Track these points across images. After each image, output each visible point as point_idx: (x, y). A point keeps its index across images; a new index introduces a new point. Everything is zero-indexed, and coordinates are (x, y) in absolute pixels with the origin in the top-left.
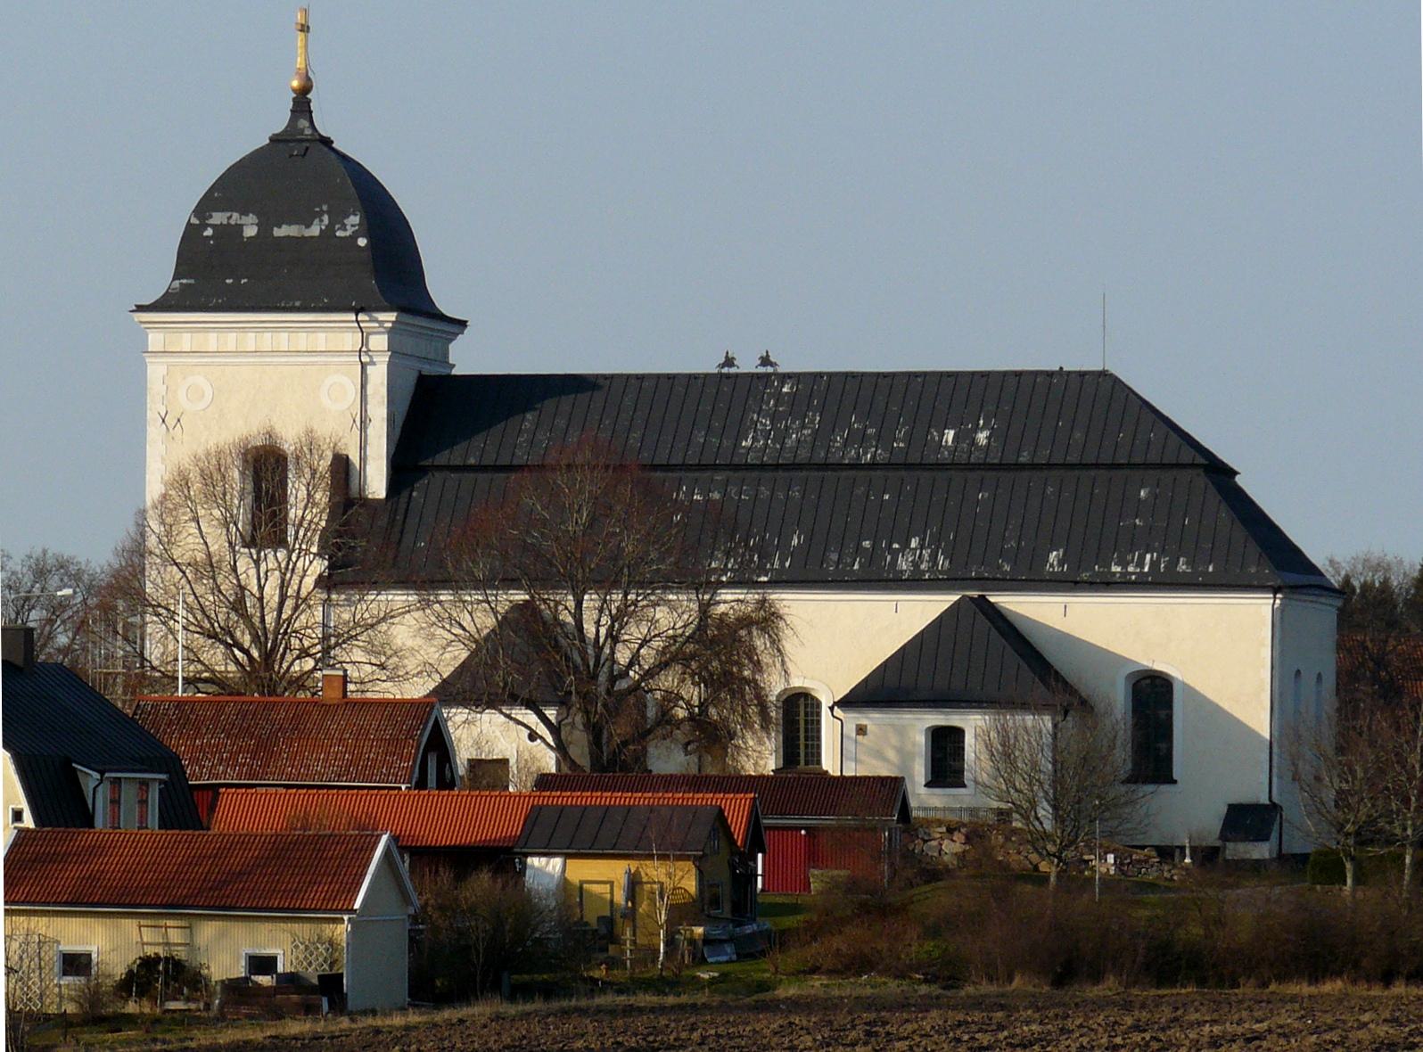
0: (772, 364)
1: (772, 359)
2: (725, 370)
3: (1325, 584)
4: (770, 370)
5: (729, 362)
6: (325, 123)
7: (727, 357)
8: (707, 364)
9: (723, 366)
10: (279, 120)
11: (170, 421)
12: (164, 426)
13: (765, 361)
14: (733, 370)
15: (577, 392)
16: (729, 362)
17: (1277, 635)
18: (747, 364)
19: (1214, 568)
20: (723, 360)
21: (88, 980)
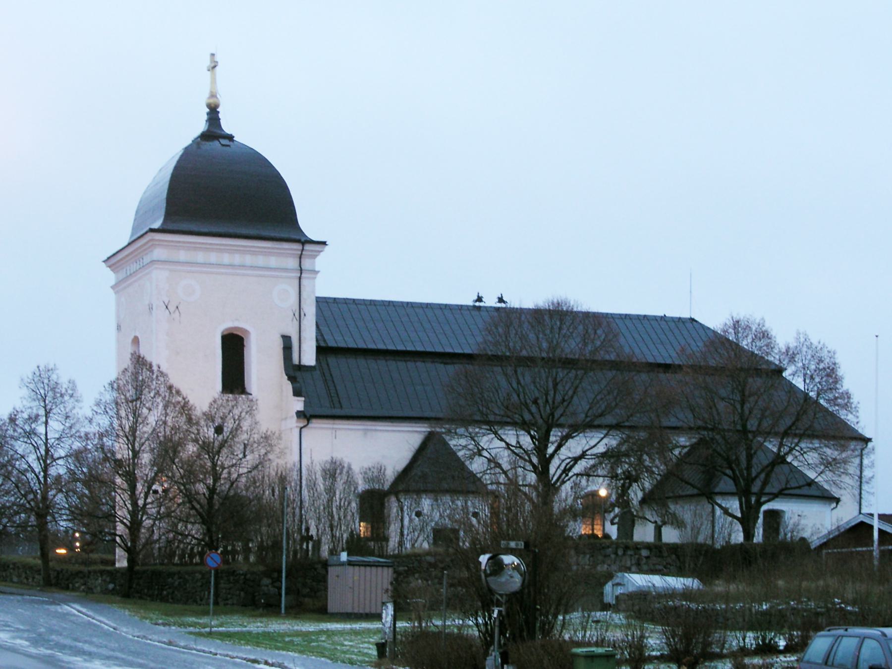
0: (504, 302)
1: (505, 299)
2: (477, 304)
3: (855, 435)
4: (503, 305)
5: (479, 299)
6: (227, 127)
7: (478, 296)
8: (468, 300)
9: (476, 301)
10: (200, 125)
11: (172, 308)
12: (177, 311)
13: (501, 300)
14: (482, 304)
15: (813, 481)
16: (479, 299)
17: (244, 231)
18: (490, 301)
19: (60, 547)
20: (476, 298)
21: (255, 564)
